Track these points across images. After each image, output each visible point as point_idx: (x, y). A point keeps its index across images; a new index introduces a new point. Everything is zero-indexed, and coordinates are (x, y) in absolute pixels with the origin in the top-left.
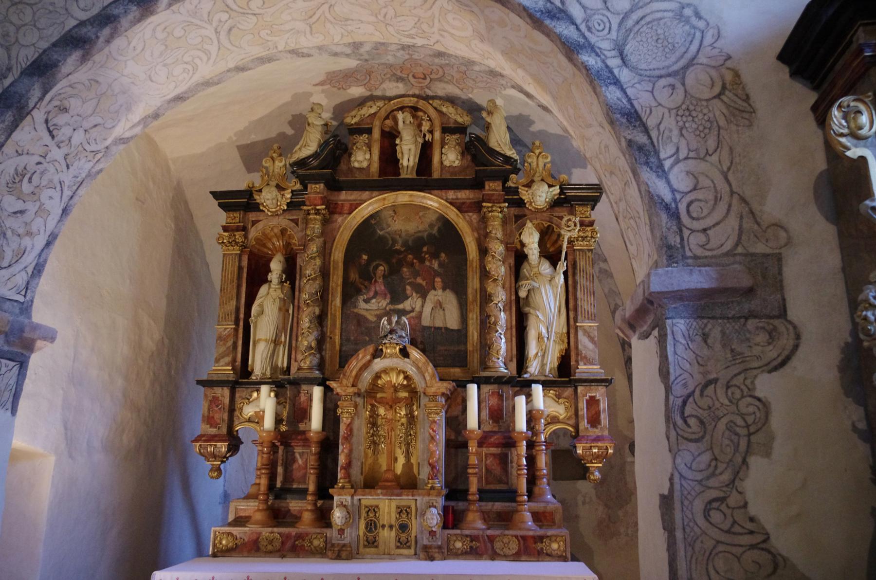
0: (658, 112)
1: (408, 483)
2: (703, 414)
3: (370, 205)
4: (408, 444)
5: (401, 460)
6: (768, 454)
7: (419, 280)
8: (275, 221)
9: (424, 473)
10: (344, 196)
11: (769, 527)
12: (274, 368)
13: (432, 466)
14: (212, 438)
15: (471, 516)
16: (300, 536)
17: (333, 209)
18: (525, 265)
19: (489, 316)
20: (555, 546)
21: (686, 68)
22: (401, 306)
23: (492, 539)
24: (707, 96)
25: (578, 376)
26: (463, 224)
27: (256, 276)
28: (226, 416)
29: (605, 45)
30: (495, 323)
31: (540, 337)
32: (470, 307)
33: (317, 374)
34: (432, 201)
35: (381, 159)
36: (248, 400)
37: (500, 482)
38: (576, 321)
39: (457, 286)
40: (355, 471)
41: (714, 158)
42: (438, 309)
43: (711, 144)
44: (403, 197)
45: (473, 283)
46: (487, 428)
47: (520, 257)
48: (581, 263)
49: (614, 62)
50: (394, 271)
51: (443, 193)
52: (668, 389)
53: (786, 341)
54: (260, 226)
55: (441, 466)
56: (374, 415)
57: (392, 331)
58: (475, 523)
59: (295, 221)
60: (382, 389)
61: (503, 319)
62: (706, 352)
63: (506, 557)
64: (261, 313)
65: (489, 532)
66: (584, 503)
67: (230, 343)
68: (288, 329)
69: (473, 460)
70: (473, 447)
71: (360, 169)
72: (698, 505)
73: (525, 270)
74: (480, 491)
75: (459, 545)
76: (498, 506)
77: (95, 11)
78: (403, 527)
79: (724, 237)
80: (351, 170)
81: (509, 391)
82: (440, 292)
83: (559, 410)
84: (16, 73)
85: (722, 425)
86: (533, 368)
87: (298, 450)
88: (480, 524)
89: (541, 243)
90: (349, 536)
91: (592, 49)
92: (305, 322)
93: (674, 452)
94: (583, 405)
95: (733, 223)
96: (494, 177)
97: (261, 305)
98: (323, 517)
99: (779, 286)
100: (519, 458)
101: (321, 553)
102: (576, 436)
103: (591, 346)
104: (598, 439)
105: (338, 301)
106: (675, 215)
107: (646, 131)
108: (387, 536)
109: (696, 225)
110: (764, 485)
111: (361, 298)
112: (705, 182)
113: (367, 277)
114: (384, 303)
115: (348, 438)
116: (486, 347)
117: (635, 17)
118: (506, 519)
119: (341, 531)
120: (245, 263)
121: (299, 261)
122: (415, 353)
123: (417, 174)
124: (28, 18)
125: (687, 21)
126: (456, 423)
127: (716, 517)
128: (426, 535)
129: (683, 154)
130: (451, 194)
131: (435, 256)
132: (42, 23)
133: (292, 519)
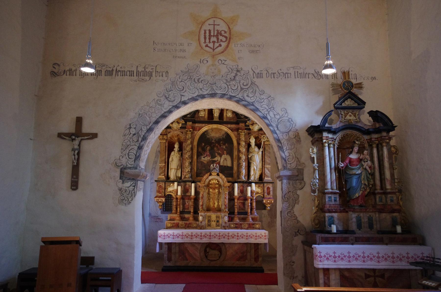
0: (284, 140)
1: (219, 210)
2: (288, 197)
3: (205, 128)
4: (218, 200)
5: (216, 204)
6: (298, 204)
7: (219, 152)
8: (176, 132)
9: (223, 207)
10: (197, 125)
11: (297, 216)
12: (177, 177)
13: (225, 205)
14: (160, 197)
15: (235, 218)
16: (190, 224)
17: (194, 129)
18: (250, 148)
19: (240, 164)
20: (257, 226)
21: (289, 132)
22: (214, 159)
23: (241, 224)
24: (293, 137)
25: (264, 181)
26: (233, 135)
27: (171, 149)
28: (163, 191)
29: (274, 125)
30: (242, 166)
31: (254, 169)
32: (234, 160)
33: (190, 179)
34: (225, 128)
35: (208, 114)
36: (170, 186)
37: (243, 210)
38: (264, 165)
39: (230, 153)
40: (204, 206)
41: (293, 150)
42: (225, 160)
43: (293, 147)
44: (215, 126)
45: (235, 153)
46: (240, 195)
47: (249, 145)
48: (267, 148)
49: (276, 129)
50: (212, 149)
51: (226, 125)
52: (282, 193)
53: (303, 185)
54: (171, 133)
55: (227, 206)
56: (209, 191)
57: (214, 169)
58: (237, 220)
59: (182, 132)
60: (211, 184)
61: (244, 164)
62: (289, 186)
63: (245, 229)
64: (173, 160)
65: (240, 223)
66: (264, 217)
67: (164, 169)
68: (181, 166)
69: (236, 204)
70: (236, 201)
71: (202, 117)
72: (286, 213)
73: (251, 150)
74: (238, 212)
75: (232, 226)
76: (242, 216)
77: (168, 110)
78: (218, 221)
79: (294, 165)
80: (199, 117)
81: (246, 185)
82: (226, 155)
83: (259, 190)
84: (152, 123)
85: (291, 199)
86: (252, 178)
87: (186, 201)
88: (238, 221)
89: (255, 142)
90: (203, 223)
91: (272, 126)
92: (187, 164)
93: (283, 204)
94: (266, 189)
95: (295, 162)
96: (242, 122)
97: (172, 158)
98: (196, 219)
99: (303, 174)
100: (248, 203)
101: (196, 228)
102: (264, 197)
103: (268, 172)
104: (269, 198)
105: (196, 157)
106: (285, 161)
107: (281, 144)
108: (213, 224)
109: (289, 163)
110: (297, 209)
111: (202, 157)
112: (291, 155)
113: (204, 150)
114: (209, 158)
115: (202, 198)
116: (239, 172)
117: (280, 120)
118: (244, 219)
119: (201, 222)
120: (167, 145)
121: (184, 145)
122: (221, 175)
123: (219, 119)
124: (154, 111)
125: (290, 122)
126: (231, 193)
127: (289, 214)
128: (224, 223)
129: (288, 148)
130: (229, 126)
131: (224, 144)
132: (157, 112)
133: (188, 219)
